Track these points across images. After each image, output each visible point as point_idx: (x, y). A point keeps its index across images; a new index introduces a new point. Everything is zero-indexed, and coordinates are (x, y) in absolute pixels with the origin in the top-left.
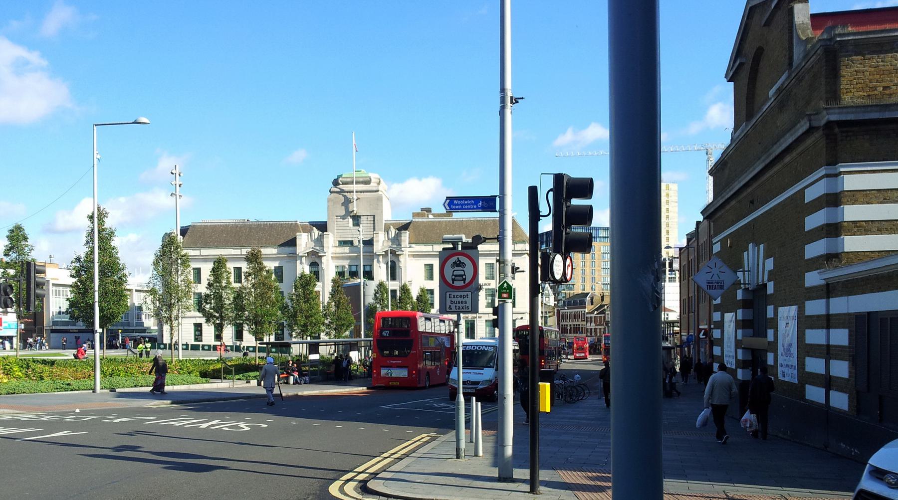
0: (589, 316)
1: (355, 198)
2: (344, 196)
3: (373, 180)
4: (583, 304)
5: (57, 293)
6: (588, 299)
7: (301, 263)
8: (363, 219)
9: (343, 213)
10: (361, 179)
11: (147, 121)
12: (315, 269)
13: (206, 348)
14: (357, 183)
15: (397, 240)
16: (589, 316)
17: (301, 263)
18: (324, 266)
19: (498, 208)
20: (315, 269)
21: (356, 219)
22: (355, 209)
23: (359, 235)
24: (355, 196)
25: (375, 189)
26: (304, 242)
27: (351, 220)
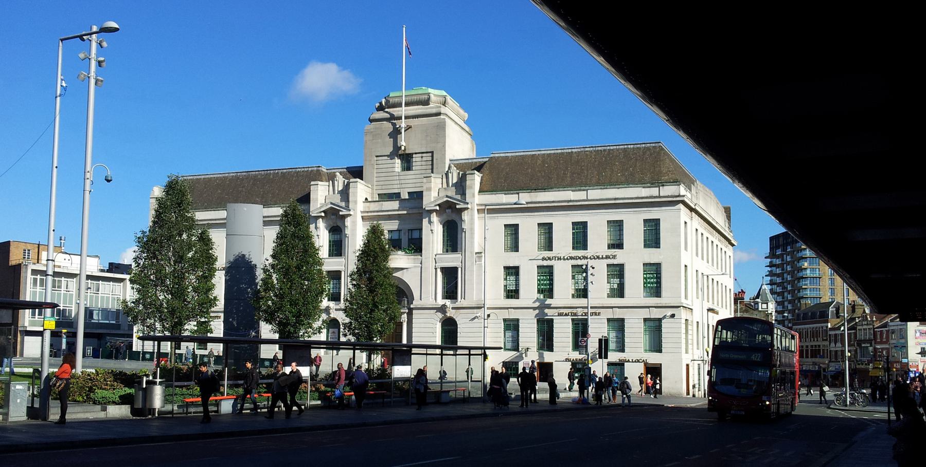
0: (832, 333)
1: (403, 125)
2: (394, 125)
3: (433, 98)
4: (824, 317)
5: (17, 247)
6: (831, 309)
7: (430, 222)
8: (416, 159)
9: (390, 149)
10: (415, 98)
11: (114, 25)
12: (337, 237)
13: (148, 356)
14: (407, 104)
15: (461, 187)
16: (832, 333)
17: (430, 222)
18: (348, 231)
19: (439, 270)
20: (337, 237)
21: (407, 160)
22: (403, 143)
23: (406, 183)
24: (403, 124)
25: (434, 111)
26: (322, 195)
27: (398, 162)
